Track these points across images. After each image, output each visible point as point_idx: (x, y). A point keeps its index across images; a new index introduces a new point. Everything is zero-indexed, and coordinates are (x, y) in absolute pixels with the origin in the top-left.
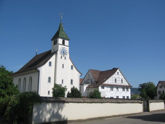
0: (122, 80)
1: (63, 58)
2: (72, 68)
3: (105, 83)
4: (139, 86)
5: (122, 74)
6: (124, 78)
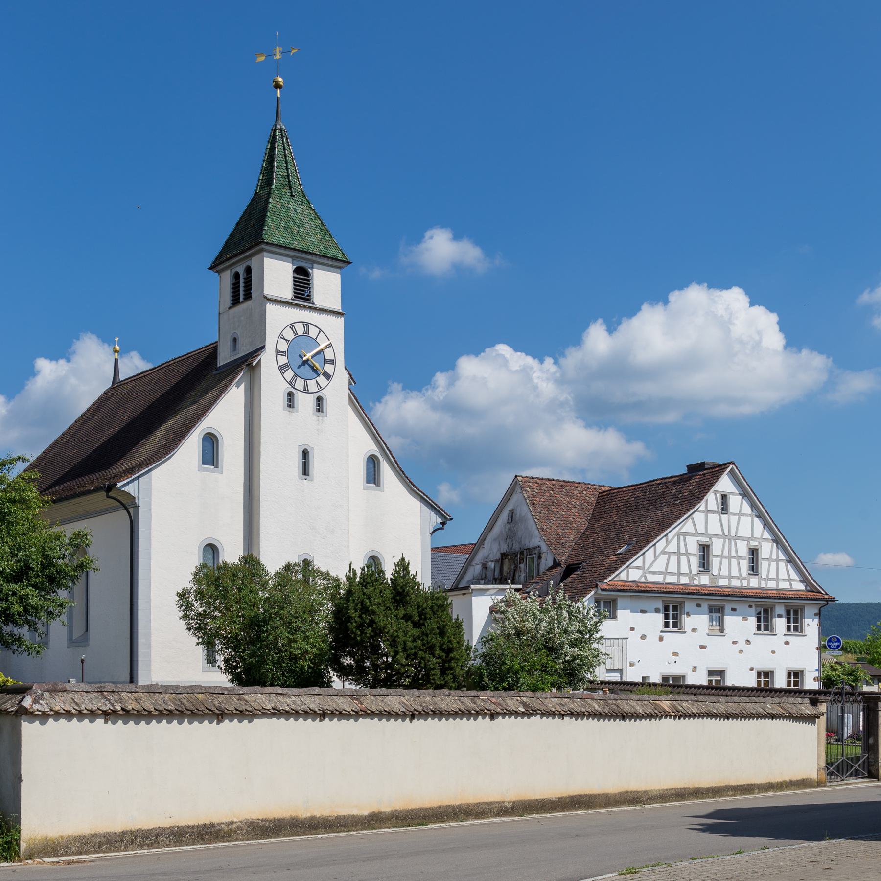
0: (754, 553)
1: (305, 402)
2: (373, 476)
3: (623, 577)
4: (600, 628)
5: (753, 506)
6: (767, 535)
